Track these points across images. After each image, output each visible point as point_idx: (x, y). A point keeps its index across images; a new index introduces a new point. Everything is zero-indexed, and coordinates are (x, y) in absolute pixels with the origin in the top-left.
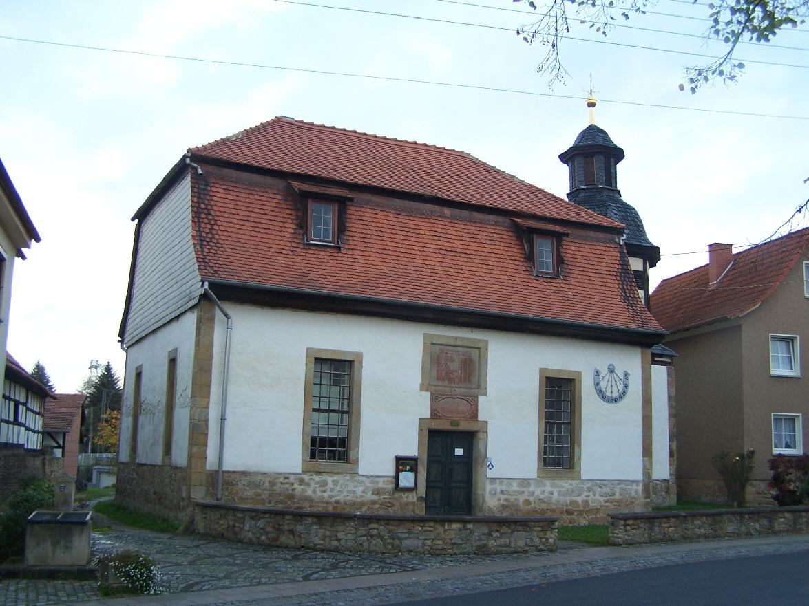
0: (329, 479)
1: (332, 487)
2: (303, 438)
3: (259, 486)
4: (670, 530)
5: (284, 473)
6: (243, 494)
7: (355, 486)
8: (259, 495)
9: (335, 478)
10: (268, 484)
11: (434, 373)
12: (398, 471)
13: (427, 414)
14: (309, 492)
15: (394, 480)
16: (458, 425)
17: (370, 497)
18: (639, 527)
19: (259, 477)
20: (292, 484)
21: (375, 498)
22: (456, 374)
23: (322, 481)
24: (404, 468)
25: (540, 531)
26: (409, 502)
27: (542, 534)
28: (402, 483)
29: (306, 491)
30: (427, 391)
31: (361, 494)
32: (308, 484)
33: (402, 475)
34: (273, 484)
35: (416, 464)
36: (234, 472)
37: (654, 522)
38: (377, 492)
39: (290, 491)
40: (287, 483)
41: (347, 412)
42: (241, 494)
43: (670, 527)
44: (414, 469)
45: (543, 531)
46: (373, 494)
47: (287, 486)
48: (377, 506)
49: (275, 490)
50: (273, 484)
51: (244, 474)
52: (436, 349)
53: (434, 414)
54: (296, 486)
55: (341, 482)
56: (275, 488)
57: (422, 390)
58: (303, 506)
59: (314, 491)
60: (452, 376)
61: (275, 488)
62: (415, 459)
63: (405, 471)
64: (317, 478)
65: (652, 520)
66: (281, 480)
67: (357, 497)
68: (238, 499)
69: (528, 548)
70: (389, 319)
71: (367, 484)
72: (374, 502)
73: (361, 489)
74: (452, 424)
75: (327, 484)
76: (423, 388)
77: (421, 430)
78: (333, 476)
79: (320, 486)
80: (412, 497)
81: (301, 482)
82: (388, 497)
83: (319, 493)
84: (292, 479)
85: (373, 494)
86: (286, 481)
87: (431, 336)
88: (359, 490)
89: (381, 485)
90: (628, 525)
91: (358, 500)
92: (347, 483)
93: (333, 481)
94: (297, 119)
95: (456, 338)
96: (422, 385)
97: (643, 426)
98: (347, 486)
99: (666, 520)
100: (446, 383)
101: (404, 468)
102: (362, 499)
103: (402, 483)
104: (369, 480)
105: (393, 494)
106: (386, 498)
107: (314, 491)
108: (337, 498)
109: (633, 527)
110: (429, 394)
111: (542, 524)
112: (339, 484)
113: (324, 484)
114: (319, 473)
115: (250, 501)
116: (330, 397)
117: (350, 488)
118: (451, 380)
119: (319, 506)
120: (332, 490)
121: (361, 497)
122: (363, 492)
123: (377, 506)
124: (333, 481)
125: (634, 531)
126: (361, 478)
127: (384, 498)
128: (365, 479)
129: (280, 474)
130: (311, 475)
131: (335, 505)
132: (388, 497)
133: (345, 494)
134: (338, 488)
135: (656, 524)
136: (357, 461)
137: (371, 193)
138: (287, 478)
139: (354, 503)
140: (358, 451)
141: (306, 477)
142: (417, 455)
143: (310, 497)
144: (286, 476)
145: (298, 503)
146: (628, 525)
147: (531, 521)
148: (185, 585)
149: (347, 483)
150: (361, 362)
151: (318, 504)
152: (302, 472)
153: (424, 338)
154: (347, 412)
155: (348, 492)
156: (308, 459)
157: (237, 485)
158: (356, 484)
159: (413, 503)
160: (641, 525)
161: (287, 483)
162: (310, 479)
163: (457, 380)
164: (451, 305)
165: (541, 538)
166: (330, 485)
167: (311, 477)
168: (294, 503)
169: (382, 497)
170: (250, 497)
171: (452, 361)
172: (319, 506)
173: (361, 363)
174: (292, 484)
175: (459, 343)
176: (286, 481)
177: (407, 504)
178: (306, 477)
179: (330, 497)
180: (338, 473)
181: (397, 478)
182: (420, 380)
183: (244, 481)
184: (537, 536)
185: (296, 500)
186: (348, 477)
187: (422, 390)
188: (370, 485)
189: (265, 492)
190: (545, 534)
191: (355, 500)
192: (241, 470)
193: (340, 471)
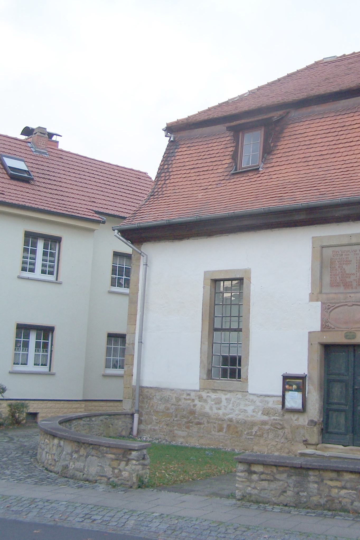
0: (223, 397)
1: (226, 405)
2: (201, 357)
3: (168, 400)
4: (343, 492)
5: (186, 390)
6: (157, 408)
7: (246, 405)
8: (168, 409)
9: (229, 395)
10: (174, 400)
11: (327, 279)
12: (284, 390)
13: (317, 327)
14: (207, 410)
15: (281, 399)
16: (354, 337)
17: (260, 417)
18: (275, 479)
19: (169, 393)
20: (193, 400)
21: (265, 418)
22: (353, 278)
23: (217, 398)
24: (290, 388)
25: (113, 460)
26: (300, 425)
27: (115, 464)
28: (289, 404)
29: (205, 408)
30: (317, 300)
31: (251, 413)
32: (206, 401)
33: (289, 395)
34: (178, 399)
35: (304, 383)
36: (151, 388)
37: (308, 476)
38: (266, 412)
39: (192, 407)
40: (189, 399)
41: (216, 330)
42: (155, 407)
43: (344, 488)
44: (301, 389)
45: (117, 460)
46: (263, 414)
47: (189, 401)
48: (267, 427)
49: (180, 405)
50: (178, 399)
51: (158, 389)
52: (328, 253)
53: (325, 327)
54: (196, 402)
55: (233, 400)
56: (180, 403)
57: (311, 300)
58: (202, 421)
59: (211, 408)
60: (348, 280)
61: (180, 403)
62: (303, 378)
63: (292, 390)
64: (213, 396)
65: (304, 472)
66: (184, 396)
67: (248, 417)
68: (153, 412)
69: (99, 478)
70: (278, 229)
71: (258, 403)
72: (264, 423)
73: (252, 408)
74: (346, 337)
75: (221, 402)
76: (313, 298)
77: (311, 344)
78: (226, 394)
79: (216, 404)
80: (303, 420)
81: (200, 398)
82: (278, 418)
83: (215, 411)
84: (193, 394)
85: (263, 414)
86: (188, 397)
87: (321, 238)
88: (250, 409)
89: (270, 405)
90: (255, 473)
91: (249, 419)
92: (238, 401)
93: (226, 399)
94: (338, 55)
95: (350, 236)
96: (312, 294)
97: (249, 323)
98: (239, 404)
99: (334, 475)
100: (342, 289)
101: (290, 388)
102: (253, 419)
103: (289, 404)
104: (260, 399)
105: (284, 416)
106: (276, 420)
107: (211, 408)
108: (230, 416)
109: (263, 477)
110: (319, 303)
111: (115, 451)
112: (231, 402)
113: (218, 402)
114: (215, 390)
115: (162, 414)
116: (231, 316)
117: (242, 407)
118: (347, 285)
119: (215, 423)
120: (226, 407)
121: (252, 416)
122: (254, 412)
123: (267, 427)
124: (226, 399)
125: (265, 484)
126: (252, 397)
127: (274, 419)
128: (255, 398)
129: (183, 390)
130: (208, 393)
131: (229, 423)
132: (278, 418)
133: (237, 412)
134: (230, 406)
135: (312, 478)
136: (247, 379)
137: (315, 105)
138: (189, 395)
139: (245, 422)
140: (248, 369)
141: (204, 394)
142: (306, 373)
143: (208, 413)
144: (189, 392)
145: (198, 419)
146: (255, 473)
147: (103, 446)
148: (28, 475)
149: (238, 401)
150: (250, 278)
151: (214, 421)
152: (200, 389)
153: (313, 243)
154: (216, 330)
155: (240, 410)
156: (205, 377)
157: (153, 399)
158: (247, 403)
159: (303, 427)
160: (278, 476)
161: (189, 399)
162: (208, 396)
163: (354, 284)
164: (352, 199)
165: (114, 468)
166: (224, 403)
167: (208, 394)
168: (195, 418)
169: (273, 418)
170: (161, 411)
171: (348, 262)
172: (215, 423)
173: (249, 279)
174: (193, 400)
175: (354, 241)
176: (188, 397)
177: (298, 427)
178: (204, 394)
179: (224, 414)
180: (230, 391)
181: (284, 397)
182: (310, 289)
183: (158, 395)
184: (110, 465)
185: (196, 416)
186: (239, 395)
187: (311, 300)
188: (260, 404)
189: (173, 406)
190: (119, 465)
191: (246, 419)
192: (155, 386)
193: (231, 389)
